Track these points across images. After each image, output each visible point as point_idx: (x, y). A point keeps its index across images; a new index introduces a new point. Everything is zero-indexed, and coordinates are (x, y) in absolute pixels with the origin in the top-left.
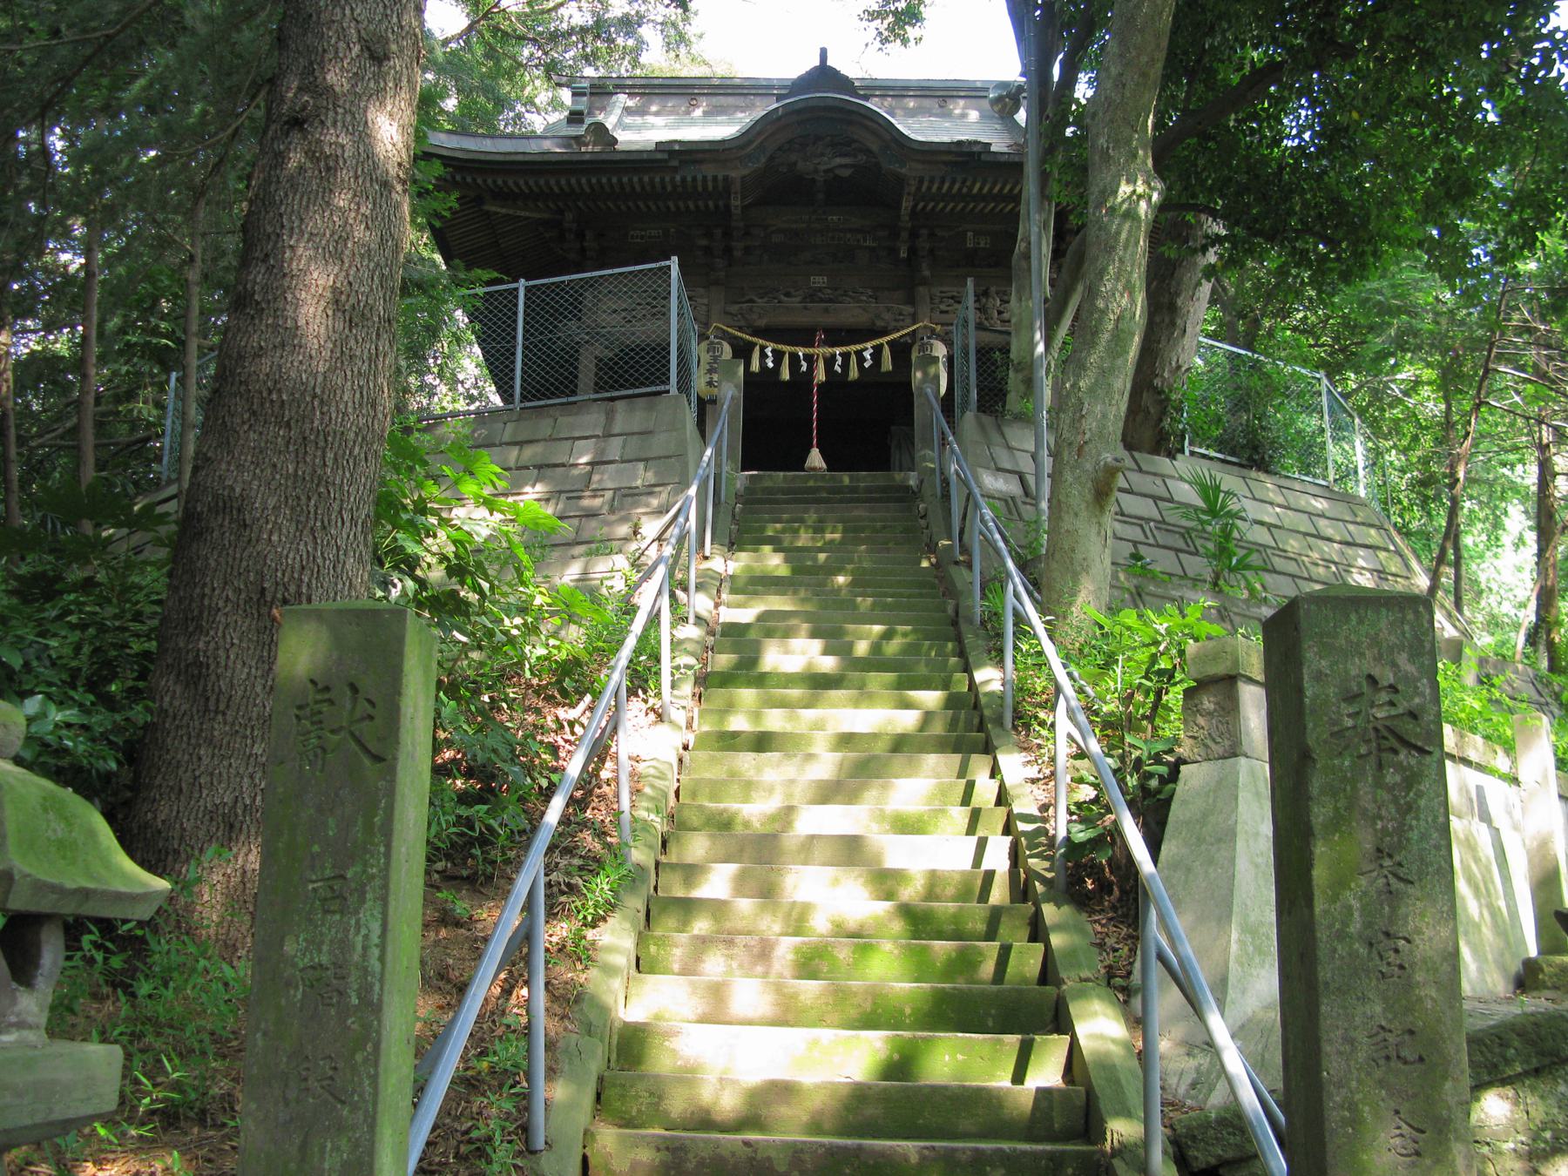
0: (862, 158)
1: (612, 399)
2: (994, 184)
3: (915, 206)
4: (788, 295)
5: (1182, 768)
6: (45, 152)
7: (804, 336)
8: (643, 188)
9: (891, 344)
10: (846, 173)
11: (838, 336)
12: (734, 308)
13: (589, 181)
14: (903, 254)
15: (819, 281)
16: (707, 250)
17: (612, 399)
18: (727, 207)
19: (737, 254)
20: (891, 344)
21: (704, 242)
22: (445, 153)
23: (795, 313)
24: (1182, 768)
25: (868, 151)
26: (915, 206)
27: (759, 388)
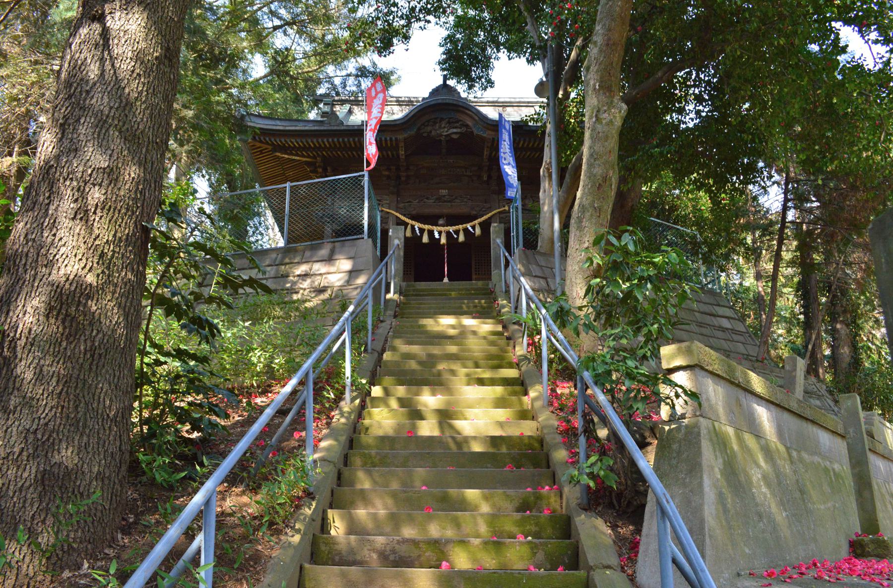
0: (464, 129)
1: (334, 242)
2: (529, 142)
3: (491, 153)
4: (427, 198)
5: (403, 227)
6: (230, 138)
7: (432, 220)
8: (392, 145)
9: (480, 224)
10: (455, 137)
11: (452, 220)
12: (401, 205)
13: (354, 140)
14: (485, 179)
15: (444, 192)
16: (388, 177)
17: (334, 242)
18: (398, 156)
19: (403, 179)
20: (480, 224)
21: (387, 173)
22: (311, 142)
23: (432, 208)
24: (403, 227)
25: (467, 126)
26: (491, 153)
27: (412, 244)
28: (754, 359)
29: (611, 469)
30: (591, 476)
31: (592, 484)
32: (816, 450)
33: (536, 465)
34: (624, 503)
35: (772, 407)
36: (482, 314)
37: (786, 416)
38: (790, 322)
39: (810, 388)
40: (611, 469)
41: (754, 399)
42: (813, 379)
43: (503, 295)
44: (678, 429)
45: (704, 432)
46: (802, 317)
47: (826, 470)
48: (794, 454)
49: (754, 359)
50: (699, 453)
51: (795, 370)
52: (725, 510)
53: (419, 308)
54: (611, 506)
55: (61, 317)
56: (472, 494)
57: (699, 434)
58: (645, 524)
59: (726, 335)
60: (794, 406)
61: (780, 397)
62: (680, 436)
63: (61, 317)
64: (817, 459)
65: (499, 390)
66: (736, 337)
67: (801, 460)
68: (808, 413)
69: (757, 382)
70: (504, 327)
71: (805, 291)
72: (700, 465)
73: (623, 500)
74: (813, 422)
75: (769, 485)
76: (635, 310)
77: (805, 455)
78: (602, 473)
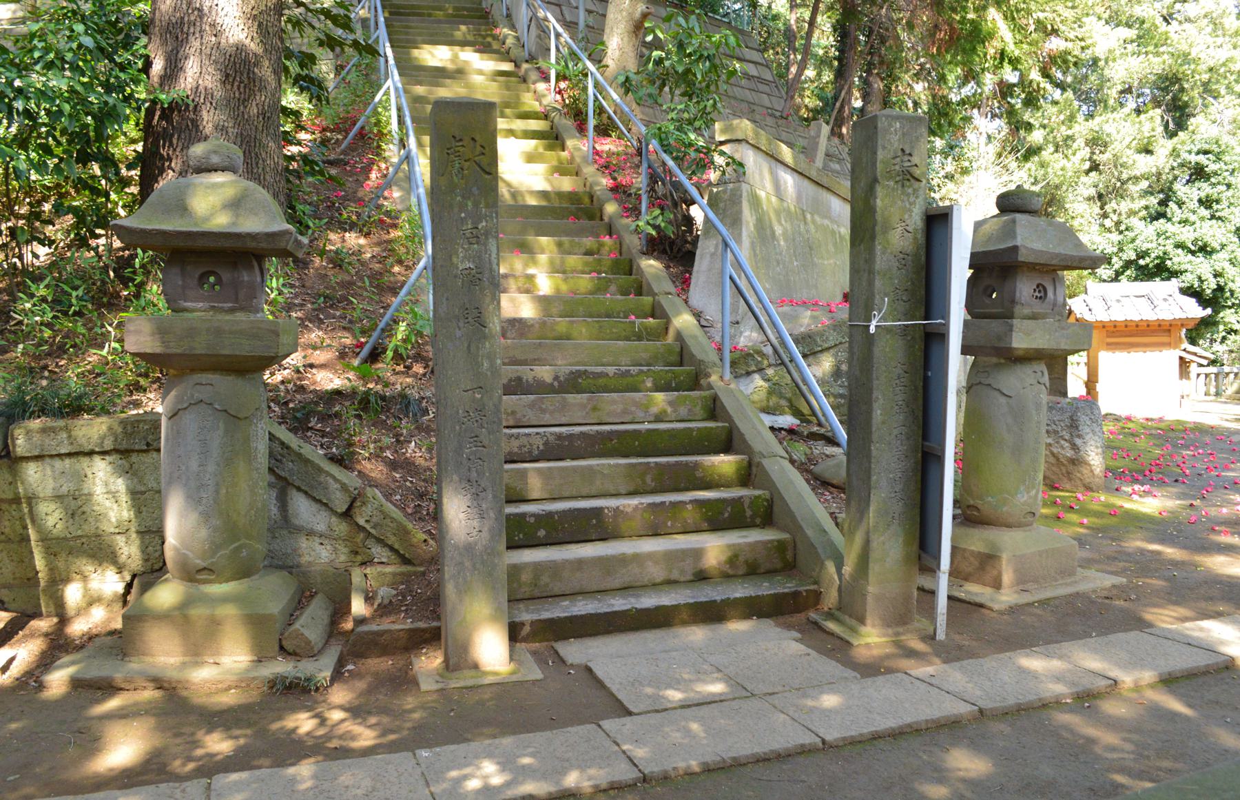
28: (778, 114)
29: (670, 222)
30: (655, 227)
31: (654, 233)
32: (827, 215)
33: (591, 218)
34: (675, 250)
35: (796, 175)
36: (484, 48)
37: (806, 183)
38: (823, 62)
39: (834, 150)
40: (670, 222)
41: (782, 167)
42: (836, 140)
43: (505, 21)
44: (725, 191)
45: (745, 194)
46: (836, 63)
47: (833, 232)
48: (809, 216)
49: (778, 114)
50: (740, 212)
51: (819, 136)
52: (755, 255)
53: (407, 34)
54: (664, 252)
55: (236, 84)
56: (544, 240)
57: (741, 196)
58: (696, 263)
59: (752, 85)
60: (813, 174)
61: (802, 167)
62: (726, 197)
63: (236, 84)
64: (826, 222)
65: (531, 144)
66: (762, 87)
67: (814, 222)
68: (824, 181)
69: (786, 153)
70: (516, 66)
71: (843, 32)
72: (740, 220)
73: (677, 249)
74: (828, 189)
75: (786, 240)
76: (691, 84)
77: (817, 218)
78: (663, 225)
